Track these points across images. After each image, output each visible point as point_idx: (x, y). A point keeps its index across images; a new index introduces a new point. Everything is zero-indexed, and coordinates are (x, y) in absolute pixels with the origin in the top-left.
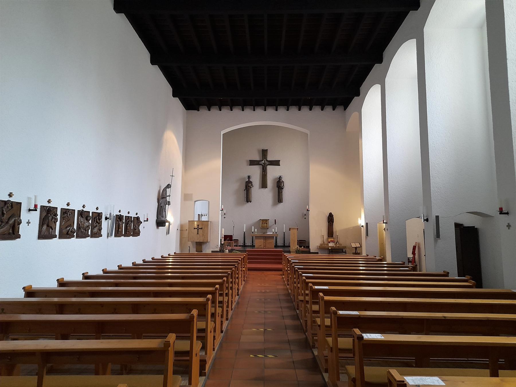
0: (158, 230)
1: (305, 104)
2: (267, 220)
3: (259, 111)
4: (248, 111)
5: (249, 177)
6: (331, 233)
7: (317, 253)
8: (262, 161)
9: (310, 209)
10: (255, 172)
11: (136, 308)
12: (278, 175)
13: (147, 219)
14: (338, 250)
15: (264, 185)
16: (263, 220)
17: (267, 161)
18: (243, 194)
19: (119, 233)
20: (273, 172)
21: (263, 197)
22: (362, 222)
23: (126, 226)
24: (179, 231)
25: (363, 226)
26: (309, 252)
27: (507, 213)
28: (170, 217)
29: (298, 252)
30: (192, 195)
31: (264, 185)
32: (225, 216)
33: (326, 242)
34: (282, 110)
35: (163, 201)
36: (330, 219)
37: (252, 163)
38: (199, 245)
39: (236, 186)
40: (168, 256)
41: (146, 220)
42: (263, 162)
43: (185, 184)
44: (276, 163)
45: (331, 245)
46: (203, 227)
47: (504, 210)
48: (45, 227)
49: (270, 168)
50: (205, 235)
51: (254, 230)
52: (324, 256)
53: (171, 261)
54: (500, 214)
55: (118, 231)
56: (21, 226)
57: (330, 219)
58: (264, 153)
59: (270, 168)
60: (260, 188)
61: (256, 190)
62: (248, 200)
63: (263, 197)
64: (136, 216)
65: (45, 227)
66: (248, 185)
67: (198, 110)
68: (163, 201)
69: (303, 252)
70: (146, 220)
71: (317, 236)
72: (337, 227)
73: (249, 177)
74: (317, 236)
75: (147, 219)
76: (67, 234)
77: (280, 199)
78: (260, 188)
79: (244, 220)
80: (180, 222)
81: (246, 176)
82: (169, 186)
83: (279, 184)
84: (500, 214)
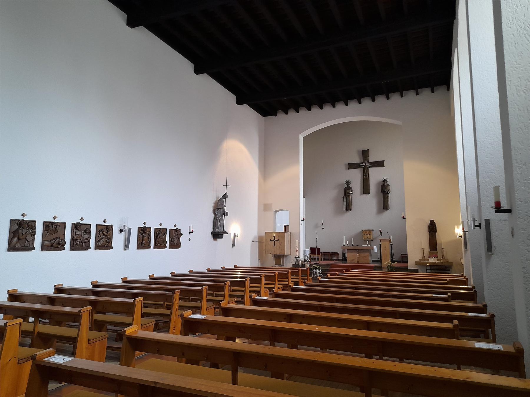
0: (215, 242)
1: (379, 94)
2: (370, 231)
3: (340, 107)
4: (328, 109)
5: (348, 183)
6: (433, 245)
7: (416, 271)
8: (363, 163)
9: (406, 217)
10: (355, 177)
11: (290, 318)
12: (382, 178)
13: (192, 231)
14: (443, 268)
15: (366, 190)
16: (365, 231)
17: (369, 162)
18: (342, 202)
19: (143, 245)
20: (376, 175)
21: (365, 204)
22: (459, 231)
23: (168, 239)
24: (256, 245)
25: (461, 236)
26: (406, 269)
27: (509, 211)
28: (233, 227)
29: (391, 269)
30: (271, 204)
31: (366, 190)
32: (323, 227)
33: (427, 257)
34: (367, 103)
35: (219, 210)
36: (432, 227)
37: (352, 166)
38: (279, 258)
39: (330, 194)
40: (234, 268)
41: (191, 231)
42: (364, 164)
43: (263, 193)
44: (380, 164)
45: (432, 260)
46: (279, 239)
47: (505, 206)
48: (15, 240)
49: (372, 171)
50: (283, 247)
51: (346, 242)
52: (423, 274)
53: (239, 276)
54: (497, 212)
55: (142, 243)
56: (182, 238)
57: (432, 227)
58: (365, 153)
59: (372, 171)
60: (361, 194)
61: (357, 197)
62: (348, 208)
63: (365, 204)
64: (175, 228)
65: (15, 240)
66: (347, 192)
67: (276, 116)
68: (219, 210)
69: (397, 269)
70: (191, 231)
71: (416, 249)
72: (442, 237)
73: (348, 183)
74: (416, 249)
75: (192, 231)
76: (52, 246)
77: (385, 206)
78: (361, 194)
79: (339, 233)
80: (258, 233)
81: (345, 181)
82: (225, 196)
83: (384, 189)
84: (497, 212)
